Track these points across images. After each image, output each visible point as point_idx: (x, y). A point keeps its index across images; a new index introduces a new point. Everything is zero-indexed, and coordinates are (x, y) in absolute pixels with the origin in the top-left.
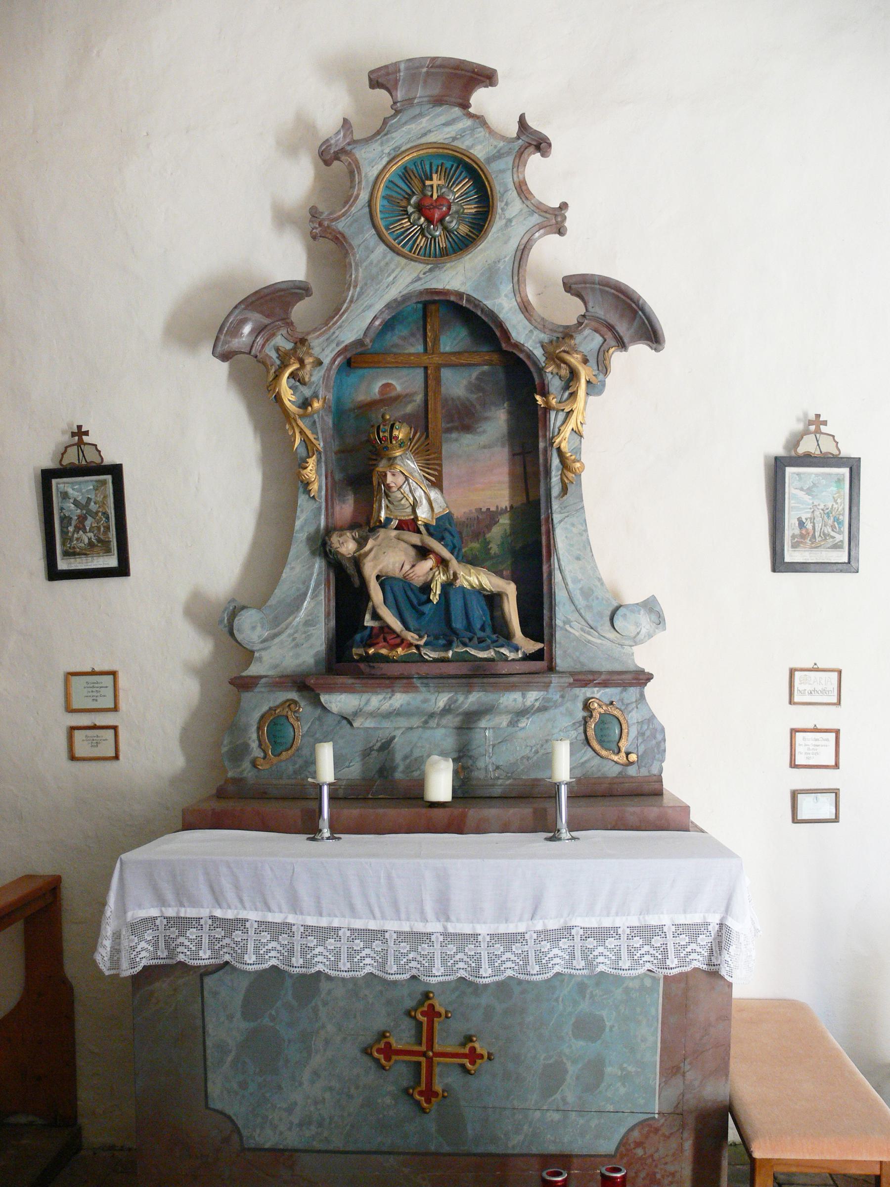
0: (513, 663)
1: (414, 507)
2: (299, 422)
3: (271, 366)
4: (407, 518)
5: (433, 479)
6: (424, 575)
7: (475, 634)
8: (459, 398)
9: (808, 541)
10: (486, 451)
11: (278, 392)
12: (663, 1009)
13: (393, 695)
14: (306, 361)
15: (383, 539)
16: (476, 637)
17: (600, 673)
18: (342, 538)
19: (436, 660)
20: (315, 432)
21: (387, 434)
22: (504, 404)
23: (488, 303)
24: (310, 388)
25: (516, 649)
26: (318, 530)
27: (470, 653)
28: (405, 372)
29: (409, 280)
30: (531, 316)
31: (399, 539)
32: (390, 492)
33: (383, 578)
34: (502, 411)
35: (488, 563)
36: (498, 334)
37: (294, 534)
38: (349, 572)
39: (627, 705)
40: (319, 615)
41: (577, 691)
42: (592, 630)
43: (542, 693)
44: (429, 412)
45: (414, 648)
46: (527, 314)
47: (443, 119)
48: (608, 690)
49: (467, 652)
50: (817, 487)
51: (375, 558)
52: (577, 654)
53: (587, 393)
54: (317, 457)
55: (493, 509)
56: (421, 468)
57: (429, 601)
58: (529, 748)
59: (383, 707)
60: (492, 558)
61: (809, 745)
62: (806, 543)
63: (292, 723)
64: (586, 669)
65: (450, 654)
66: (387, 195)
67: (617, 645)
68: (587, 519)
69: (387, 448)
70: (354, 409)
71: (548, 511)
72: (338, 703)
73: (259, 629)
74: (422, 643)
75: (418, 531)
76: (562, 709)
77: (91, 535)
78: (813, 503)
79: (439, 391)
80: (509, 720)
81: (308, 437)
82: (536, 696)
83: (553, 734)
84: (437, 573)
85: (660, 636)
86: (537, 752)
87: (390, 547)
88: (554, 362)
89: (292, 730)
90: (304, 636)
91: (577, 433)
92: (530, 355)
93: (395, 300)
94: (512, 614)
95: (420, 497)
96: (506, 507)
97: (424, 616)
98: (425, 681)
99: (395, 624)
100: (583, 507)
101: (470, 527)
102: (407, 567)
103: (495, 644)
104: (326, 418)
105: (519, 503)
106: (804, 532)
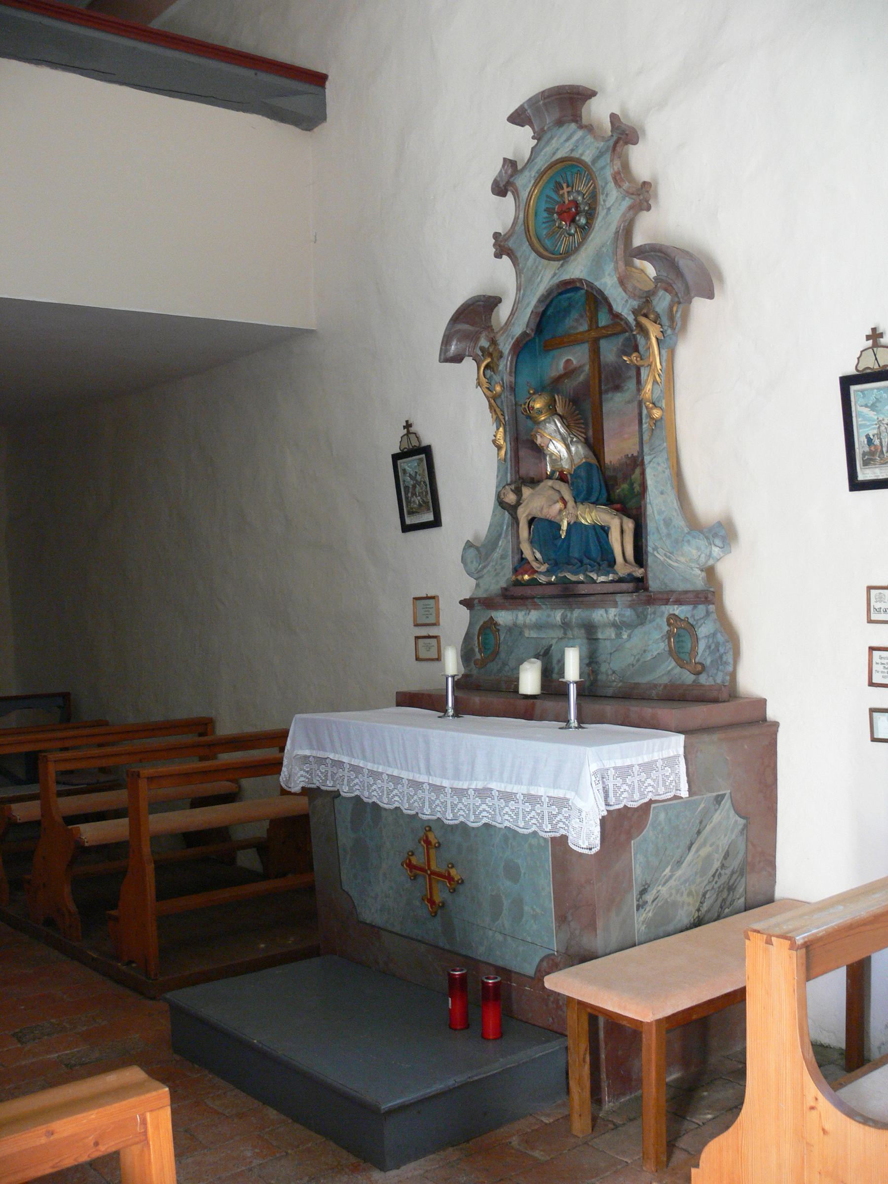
9: (877, 458)
12: (552, 866)
23: (597, 284)
29: (550, 276)
39: (698, 620)
47: (564, 137)
50: (880, 402)
52: (663, 576)
58: (633, 657)
61: (884, 664)
62: (876, 459)
65: (553, 578)
66: (547, 208)
76: (654, 624)
77: (419, 498)
78: (878, 418)
86: (638, 660)
90: (500, 567)
93: (543, 295)
106: (873, 448)
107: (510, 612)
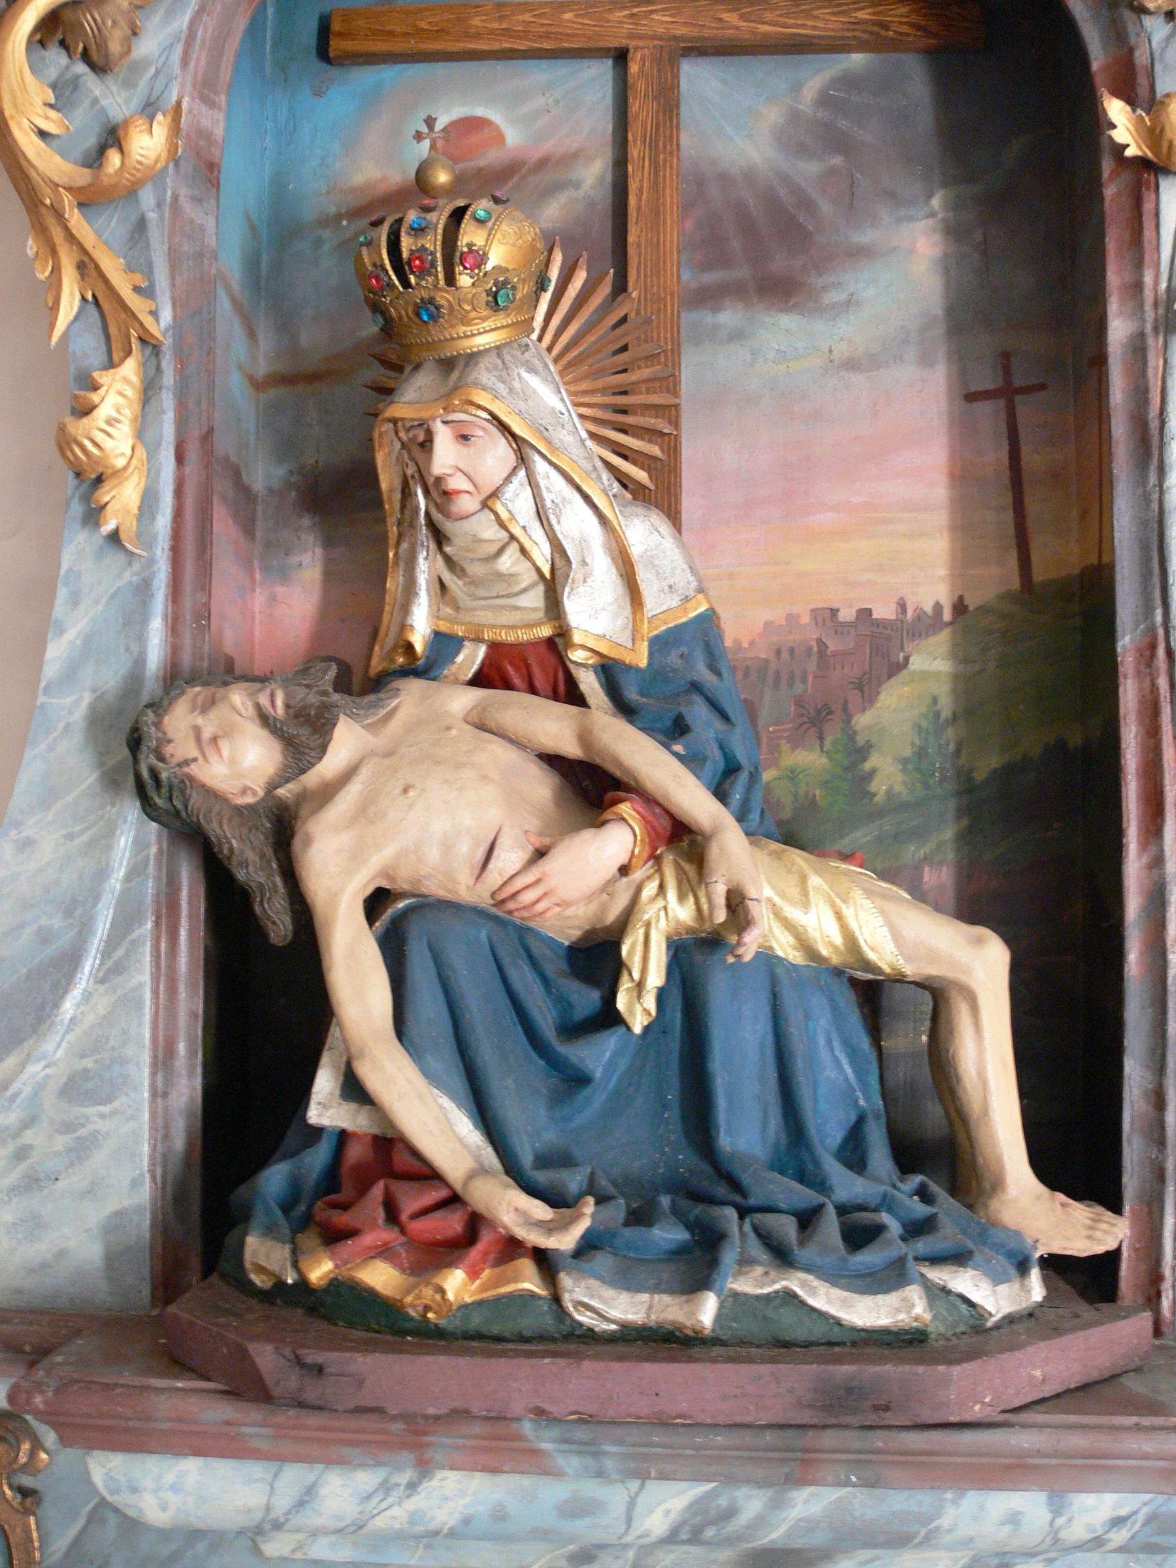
2: (75, 218)
4: (524, 636)
5: (641, 475)
6: (590, 898)
7: (821, 1185)
8: (750, 176)
10: (857, 379)
15: (418, 724)
18: (214, 714)
20: (139, 264)
21: (433, 243)
22: (930, 195)
24: (129, 84)
26: (135, 678)
27: (803, 1303)
28: (540, 73)
31: (482, 727)
33: (401, 905)
35: (862, 836)
37: (41, 699)
38: (240, 875)
40: (129, 1052)
45: (527, 1266)
49: (789, 1297)
51: (364, 812)
54: (144, 365)
55: (884, 611)
56: (593, 428)
57: (609, 1018)
60: (878, 814)
70: (339, 217)
72: (170, 1496)
74: (565, 1242)
75: (573, 696)
79: (672, 139)
84: (650, 889)
87: (437, 763)
90: (61, 1142)
94: (992, 1084)
95: (583, 542)
96: (938, 607)
97: (587, 1092)
101: (791, 684)
102: (509, 859)
103: (922, 1246)
107: (256, 1469)
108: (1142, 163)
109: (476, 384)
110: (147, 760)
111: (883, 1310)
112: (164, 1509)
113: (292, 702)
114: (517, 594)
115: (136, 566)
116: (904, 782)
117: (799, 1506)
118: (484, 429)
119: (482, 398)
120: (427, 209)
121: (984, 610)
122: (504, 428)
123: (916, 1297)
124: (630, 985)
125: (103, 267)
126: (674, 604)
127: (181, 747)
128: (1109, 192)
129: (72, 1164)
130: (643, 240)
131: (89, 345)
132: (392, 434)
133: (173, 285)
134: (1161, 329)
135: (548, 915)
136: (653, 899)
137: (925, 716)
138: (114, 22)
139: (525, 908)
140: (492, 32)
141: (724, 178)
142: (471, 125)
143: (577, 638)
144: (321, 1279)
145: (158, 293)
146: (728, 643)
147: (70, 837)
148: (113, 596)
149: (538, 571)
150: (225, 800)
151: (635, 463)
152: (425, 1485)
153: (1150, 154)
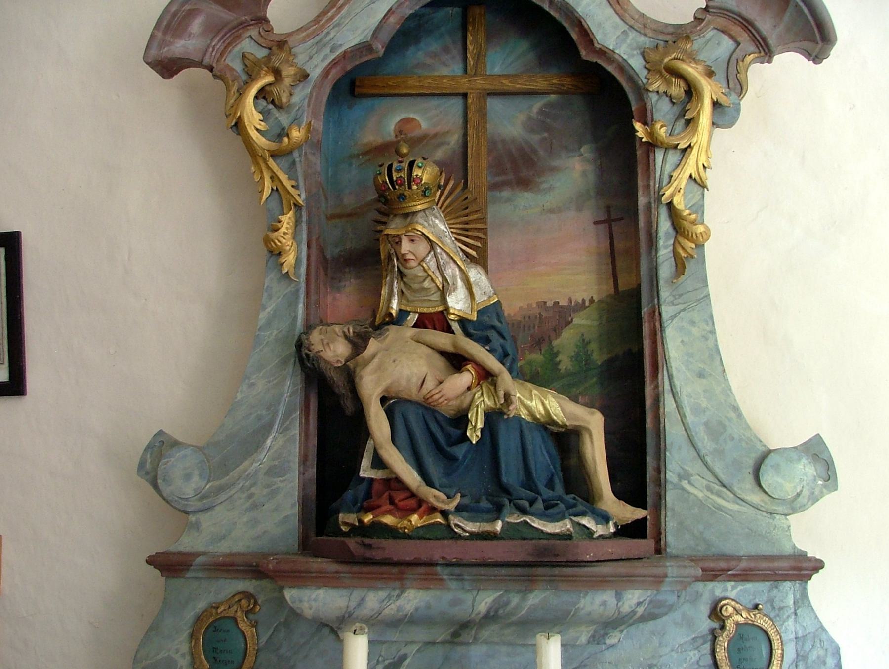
0: (604, 542)
1: (443, 293)
3: (233, 81)
4: (431, 310)
5: (474, 253)
7: (539, 493)
10: (553, 216)
11: (240, 117)
13: (402, 592)
14: (284, 73)
16: (540, 499)
17: (739, 559)
19: (474, 536)
21: (404, 174)
24: (288, 112)
25: (604, 518)
28: (434, 102)
30: (625, 11)
32: (406, 268)
34: (578, 158)
35: (556, 384)
36: (574, 36)
41: (700, 586)
42: (724, 490)
43: (649, 593)
44: (469, 158)
45: (438, 515)
46: (618, 8)
48: (749, 585)
49: (526, 523)
51: (380, 368)
52: (701, 527)
53: (713, 124)
55: (563, 302)
56: (456, 236)
57: (465, 439)
59: (386, 611)
63: (243, 629)
64: (714, 550)
65: (499, 526)
67: (764, 514)
68: (714, 313)
69: (402, 197)
70: (358, 155)
71: (653, 300)
73: (196, 478)
75: (449, 330)
76: (676, 615)
80: (591, 633)
81: (283, 184)
82: (639, 598)
83: (661, 656)
85: (828, 500)
88: (661, 75)
89: (242, 640)
90: (265, 491)
91: (698, 183)
92: (623, 67)
94: (598, 461)
95: (454, 277)
96: (584, 301)
98: (457, 570)
99: (410, 476)
100: (708, 296)
101: (529, 329)
102: (430, 384)
103: (571, 510)
104: (312, 158)
105: (604, 295)
107: (344, 592)
108: (647, 143)
109: (417, 222)
110: (304, 351)
111: (557, 527)
112: (311, 609)
113: (356, 331)
114: (429, 296)
115: (293, 286)
116: (571, 365)
117: (531, 600)
118: (420, 238)
119: (419, 228)
120: (400, 162)
121: (600, 301)
122: (427, 238)
123: (568, 522)
124: (471, 427)
125: (281, 178)
126: (486, 299)
127: (317, 346)
128: (639, 152)
129: (269, 499)
130: (473, 165)
131: (274, 205)
132: (386, 239)
133: (305, 185)
134: (657, 201)
135: (443, 404)
136: (479, 398)
137: (579, 341)
138: (284, 91)
139: (435, 401)
140: (417, 87)
141: (503, 141)
142: (408, 121)
143: (452, 311)
144: (369, 521)
145: (300, 187)
146: (506, 314)
147: (269, 382)
148: (284, 296)
149: (438, 287)
150: (332, 365)
151: (471, 249)
152: (403, 595)
153: (651, 141)
